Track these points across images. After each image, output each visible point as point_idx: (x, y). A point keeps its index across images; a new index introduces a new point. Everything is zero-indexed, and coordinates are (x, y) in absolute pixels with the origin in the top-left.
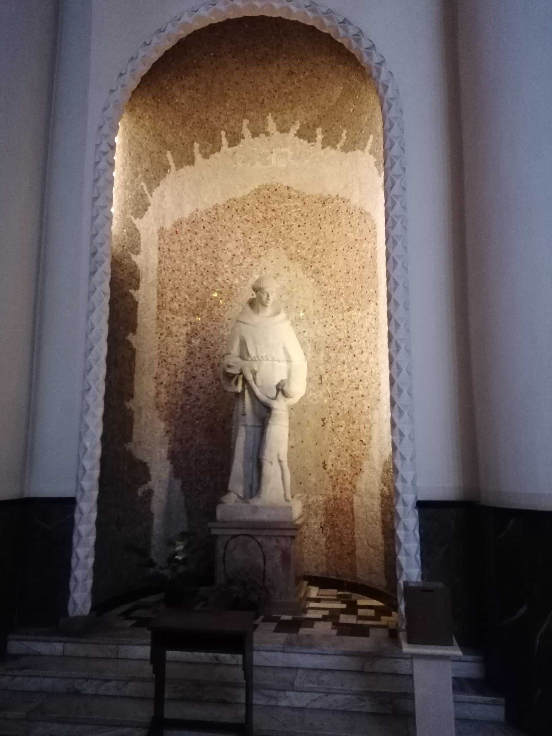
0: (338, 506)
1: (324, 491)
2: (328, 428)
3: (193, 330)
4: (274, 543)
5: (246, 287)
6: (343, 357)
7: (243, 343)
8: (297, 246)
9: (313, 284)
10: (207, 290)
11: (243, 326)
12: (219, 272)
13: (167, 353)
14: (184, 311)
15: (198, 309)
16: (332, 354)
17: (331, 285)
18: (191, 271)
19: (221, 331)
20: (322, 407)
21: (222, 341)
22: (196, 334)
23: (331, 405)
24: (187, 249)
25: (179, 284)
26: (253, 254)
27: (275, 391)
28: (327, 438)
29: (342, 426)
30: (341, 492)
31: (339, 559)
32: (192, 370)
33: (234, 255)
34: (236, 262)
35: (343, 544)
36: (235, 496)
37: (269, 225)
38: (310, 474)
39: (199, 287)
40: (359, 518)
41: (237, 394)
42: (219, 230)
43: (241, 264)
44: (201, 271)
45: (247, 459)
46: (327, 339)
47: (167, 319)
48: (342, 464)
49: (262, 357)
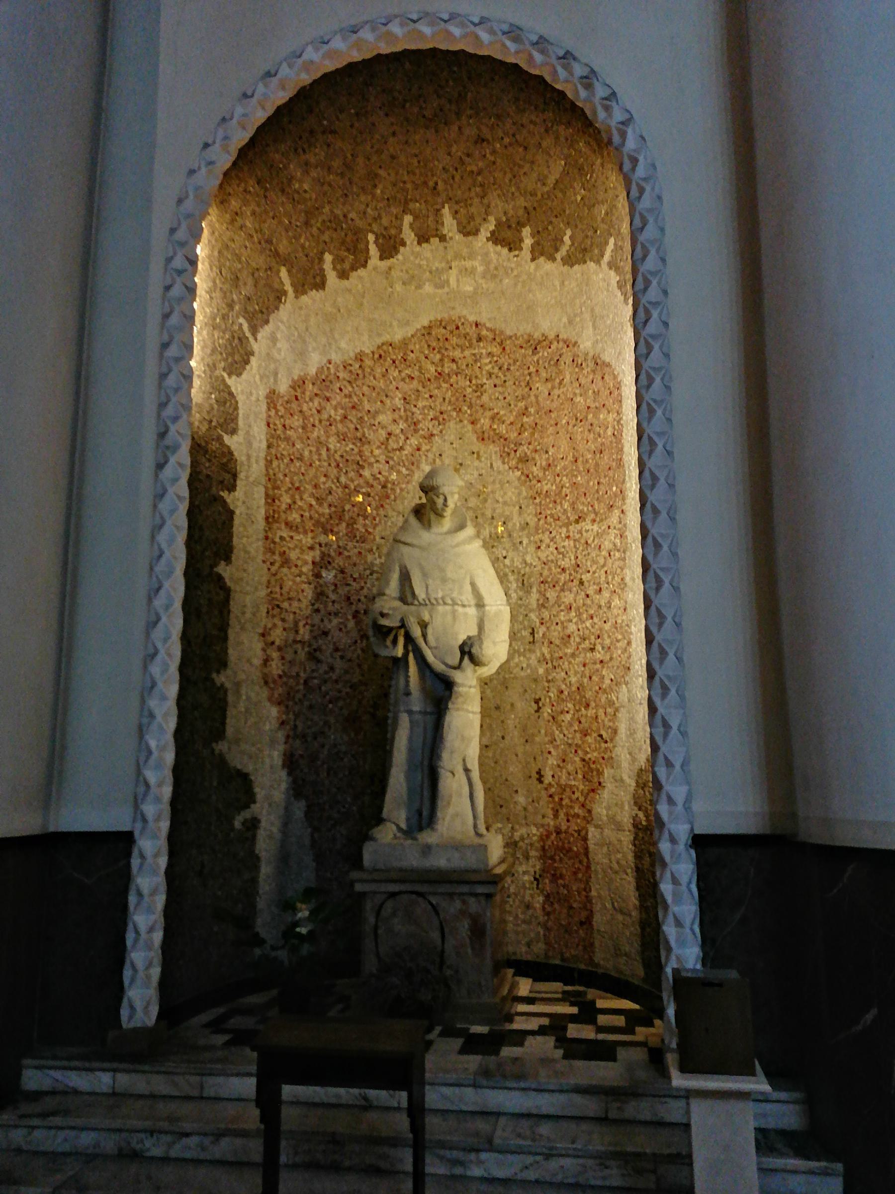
4: (458, 904)
6: (568, 598)
9: (519, 479)
10: (347, 490)
11: (405, 550)
12: (365, 461)
13: (281, 594)
14: (309, 525)
15: (332, 522)
16: (551, 594)
17: (549, 480)
18: (319, 460)
19: (370, 558)
20: (535, 680)
22: (329, 562)
23: (550, 678)
24: (314, 426)
26: (421, 432)
28: (543, 731)
29: (568, 712)
30: (568, 821)
32: (322, 620)
33: (390, 434)
34: (392, 444)
35: (571, 907)
36: (394, 828)
38: (517, 791)
39: (333, 486)
40: (598, 863)
41: (395, 660)
43: (401, 449)
44: (335, 460)
45: (412, 767)
46: (542, 568)
47: (281, 538)
48: (569, 774)
49: (436, 599)
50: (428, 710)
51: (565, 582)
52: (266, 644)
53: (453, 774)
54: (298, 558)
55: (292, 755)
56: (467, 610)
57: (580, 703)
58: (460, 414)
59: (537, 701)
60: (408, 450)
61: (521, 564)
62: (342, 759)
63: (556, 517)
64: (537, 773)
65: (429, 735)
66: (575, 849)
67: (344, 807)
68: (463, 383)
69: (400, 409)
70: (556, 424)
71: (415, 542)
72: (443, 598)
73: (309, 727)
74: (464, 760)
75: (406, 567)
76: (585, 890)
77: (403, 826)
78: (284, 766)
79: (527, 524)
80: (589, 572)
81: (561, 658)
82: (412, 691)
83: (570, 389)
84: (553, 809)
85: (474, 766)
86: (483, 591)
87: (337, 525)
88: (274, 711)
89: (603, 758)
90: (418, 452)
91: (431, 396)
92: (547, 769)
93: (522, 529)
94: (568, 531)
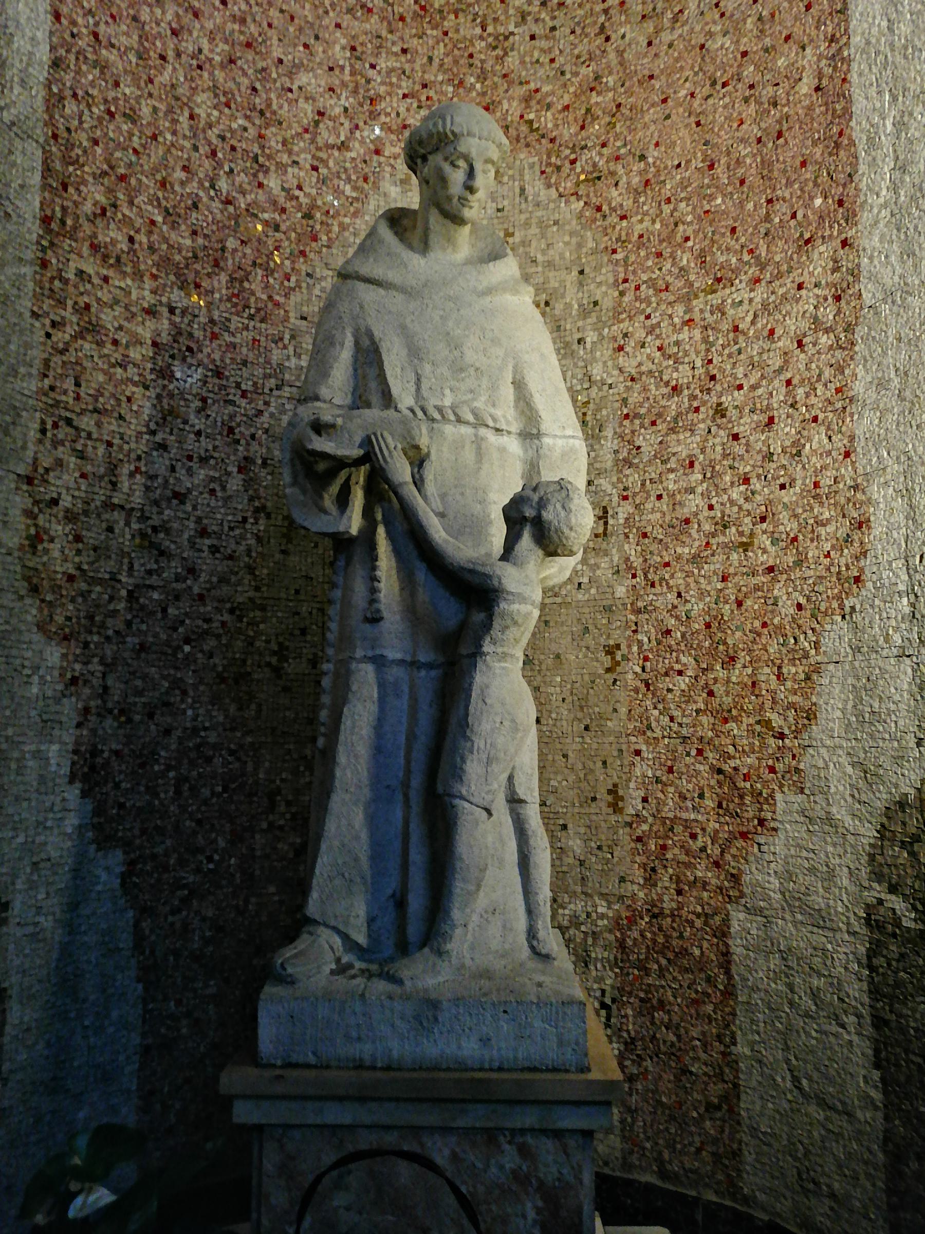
0: (667, 937)
1: (612, 886)
2: (630, 676)
3: (177, 333)
4: (510, 1158)
5: (358, 221)
6: (684, 445)
7: (369, 356)
8: (527, 100)
9: (580, 216)
10: (231, 209)
11: (368, 294)
12: (269, 157)
13: (78, 398)
14: (147, 263)
15: (197, 266)
16: (647, 441)
17: (646, 214)
18: (174, 133)
19: (276, 355)
20: (608, 609)
21: (278, 388)
22: (189, 349)
23: (640, 604)
24: (163, 58)
25: (130, 165)
26: (383, 118)
27: (498, 532)
28: (623, 710)
29: (680, 673)
30: (679, 892)
31: (672, 1118)
32: (173, 469)
33: (321, 114)
34: (325, 135)
35: (685, 1071)
36: (337, 941)
37: (435, 32)
38: (564, 827)
39: (201, 193)
40: (755, 989)
41: (342, 543)
42: (275, 23)
43: (343, 146)
44: (210, 143)
45: (381, 791)
46: (628, 389)
47: (80, 273)
48: (683, 798)
49: (440, 410)
50: (422, 658)
51: (679, 414)
52: (36, 502)
53: (489, 812)
54: (120, 328)
55: (95, 752)
56: (505, 440)
57: (712, 653)
58: (461, 90)
59: (610, 651)
60: (357, 150)
61: (581, 381)
62: (209, 760)
63: (661, 284)
64: (610, 792)
65: (426, 715)
66: (697, 952)
67: (210, 859)
68: (468, 30)
69: (342, 68)
70: (664, 101)
71: (392, 276)
72: (453, 408)
73: (139, 693)
74: (511, 778)
75: (371, 336)
76: (719, 1038)
77: (362, 939)
78: (72, 779)
79: (596, 303)
80: (740, 387)
81: (667, 565)
82: (385, 614)
83: (698, 28)
84: (644, 866)
85: (529, 789)
86: (540, 402)
87: (209, 275)
88: (54, 655)
89: (772, 770)
90: (375, 157)
91: (404, 51)
92: (632, 785)
93: (584, 313)
94: (689, 310)
